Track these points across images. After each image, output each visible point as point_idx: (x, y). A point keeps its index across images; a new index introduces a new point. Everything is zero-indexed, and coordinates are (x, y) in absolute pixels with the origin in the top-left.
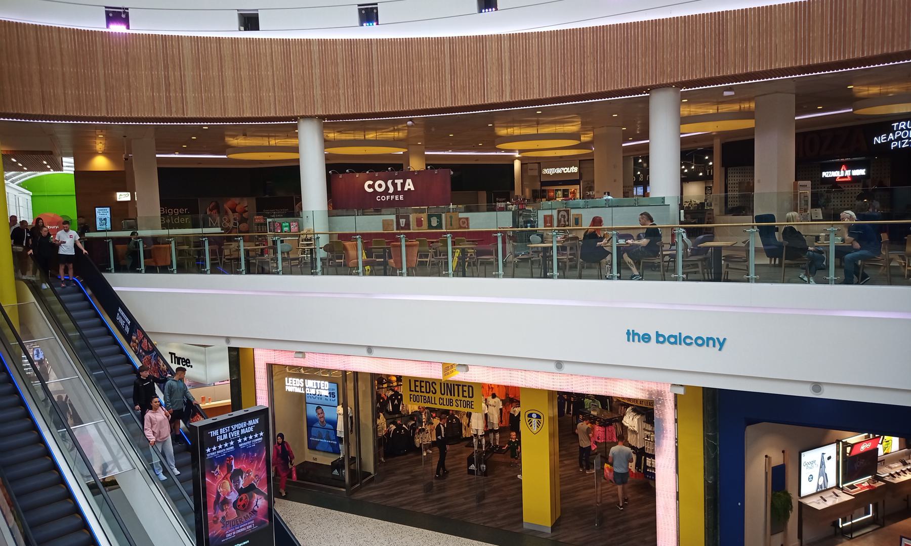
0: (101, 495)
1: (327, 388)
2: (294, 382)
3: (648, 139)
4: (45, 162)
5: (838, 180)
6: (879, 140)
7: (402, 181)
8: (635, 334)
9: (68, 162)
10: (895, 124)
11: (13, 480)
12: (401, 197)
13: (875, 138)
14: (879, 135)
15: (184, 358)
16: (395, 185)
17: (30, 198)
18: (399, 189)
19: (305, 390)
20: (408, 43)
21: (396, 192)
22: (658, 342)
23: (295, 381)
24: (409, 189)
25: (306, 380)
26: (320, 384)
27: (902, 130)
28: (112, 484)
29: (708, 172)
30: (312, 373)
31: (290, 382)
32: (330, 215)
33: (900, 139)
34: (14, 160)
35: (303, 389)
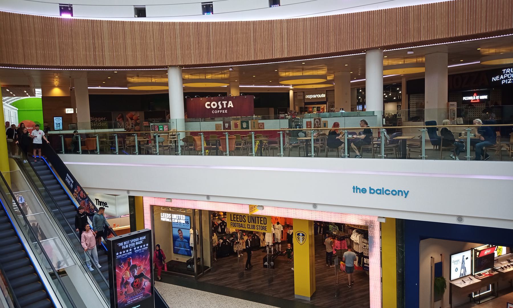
0: (57, 279)
1: (184, 219)
2: (165, 216)
3: (365, 79)
4: (25, 92)
5: (472, 101)
6: (495, 79)
7: (226, 102)
8: (357, 188)
9: (38, 92)
10: (504, 70)
11: (7, 271)
12: (226, 111)
13: (493, 78)
14: (495, 76)
15: (103, 202)
16: (222, 104)
17: (17, 112)
18: (225, 107)
19: (172, 220)
20: (230, 24)
21: (223, 108)
22: (370, 193)
23: (166, 215)
24: (230, 107)
25: (172, 215)
26: (180, 216)
27: (508, 73)
28: (63, 273)
29: (399, 97)
30: (176, 210)
31: (163, 215)
32: (186, 121)
33: (507, 78)
34: (8, 90)
35: (170, 219)
